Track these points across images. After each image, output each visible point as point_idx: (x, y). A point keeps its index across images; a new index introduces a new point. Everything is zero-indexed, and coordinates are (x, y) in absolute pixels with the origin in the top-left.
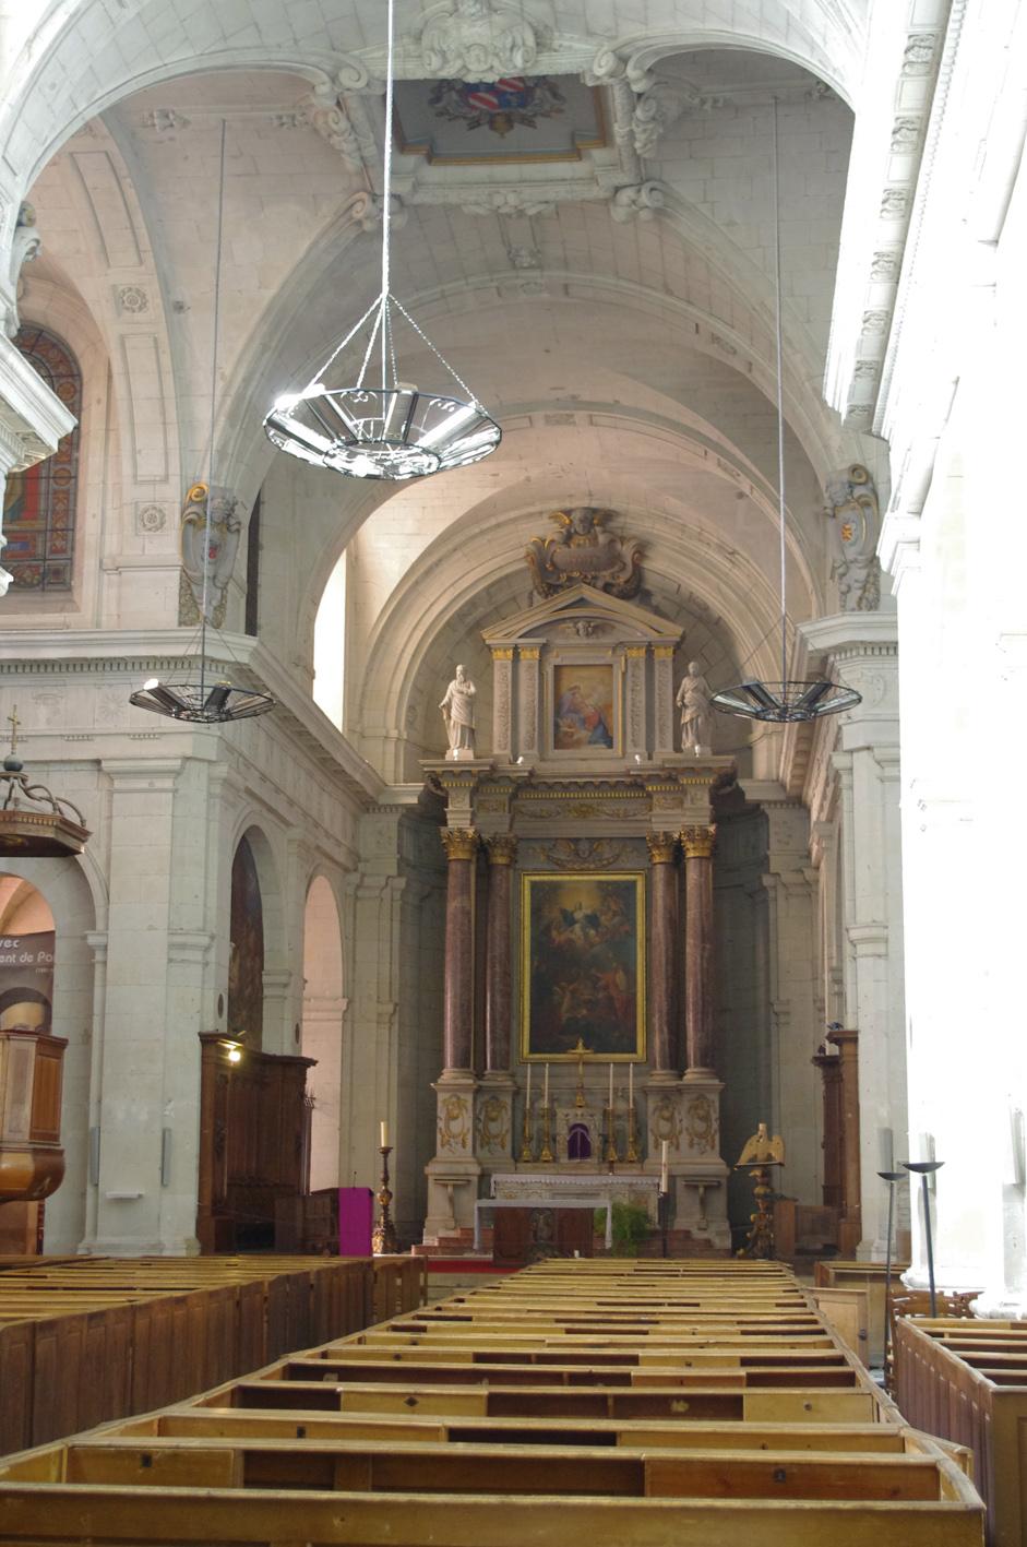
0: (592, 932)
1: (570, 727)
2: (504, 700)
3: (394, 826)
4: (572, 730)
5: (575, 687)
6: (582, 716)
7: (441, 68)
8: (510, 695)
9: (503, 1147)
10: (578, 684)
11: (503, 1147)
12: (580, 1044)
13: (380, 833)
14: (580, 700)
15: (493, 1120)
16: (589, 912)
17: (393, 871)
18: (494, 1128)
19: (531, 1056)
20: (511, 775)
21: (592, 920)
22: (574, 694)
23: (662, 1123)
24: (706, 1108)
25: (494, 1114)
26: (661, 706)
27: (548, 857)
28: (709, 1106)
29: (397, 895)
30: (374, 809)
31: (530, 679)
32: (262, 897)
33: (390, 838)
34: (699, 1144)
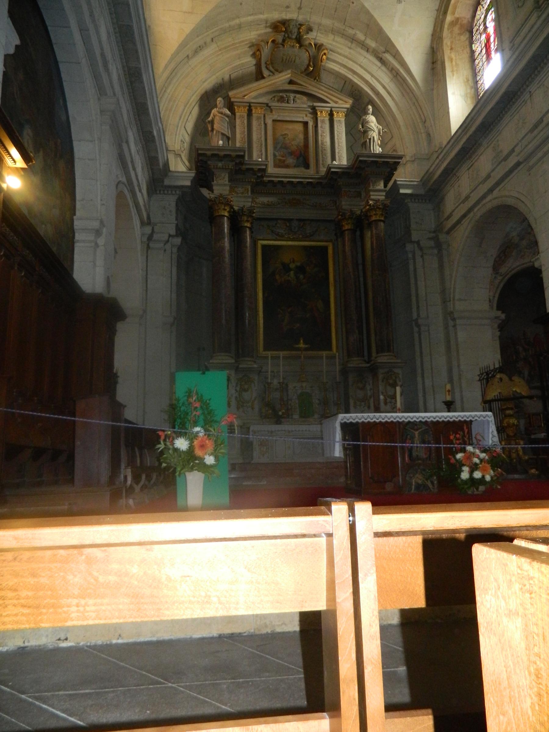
0: (301, 276)
1: (283, 157)
2: (242, 136)
3: (173, 204)
4: (284, 158)
5: (286, 134)
6: (290, 151)
7: (123, 183)
8: (246, 133)
9: (253, 409)
10: (286, 132)
11: (253, 409)
12: (302, 341)
13: (164, 208)
14: (288, 142)
15: (246, 390)
16: (299, 264)
17: (173, 232)
18: (246, 396)
19: (264, 353)
20: (254, 167)
21: (301, 269)
22: (284, 138)
23: (389, 388)
24: (394, 378)
25: (246, 387)
26: (339, 146)
27: (272, 231)
28: (396, 378)
29: (175, 250)
30: (160, 191)
31: (259, 125)
32: (75, 144)
33: (170, 211)
34: (391, 402)
